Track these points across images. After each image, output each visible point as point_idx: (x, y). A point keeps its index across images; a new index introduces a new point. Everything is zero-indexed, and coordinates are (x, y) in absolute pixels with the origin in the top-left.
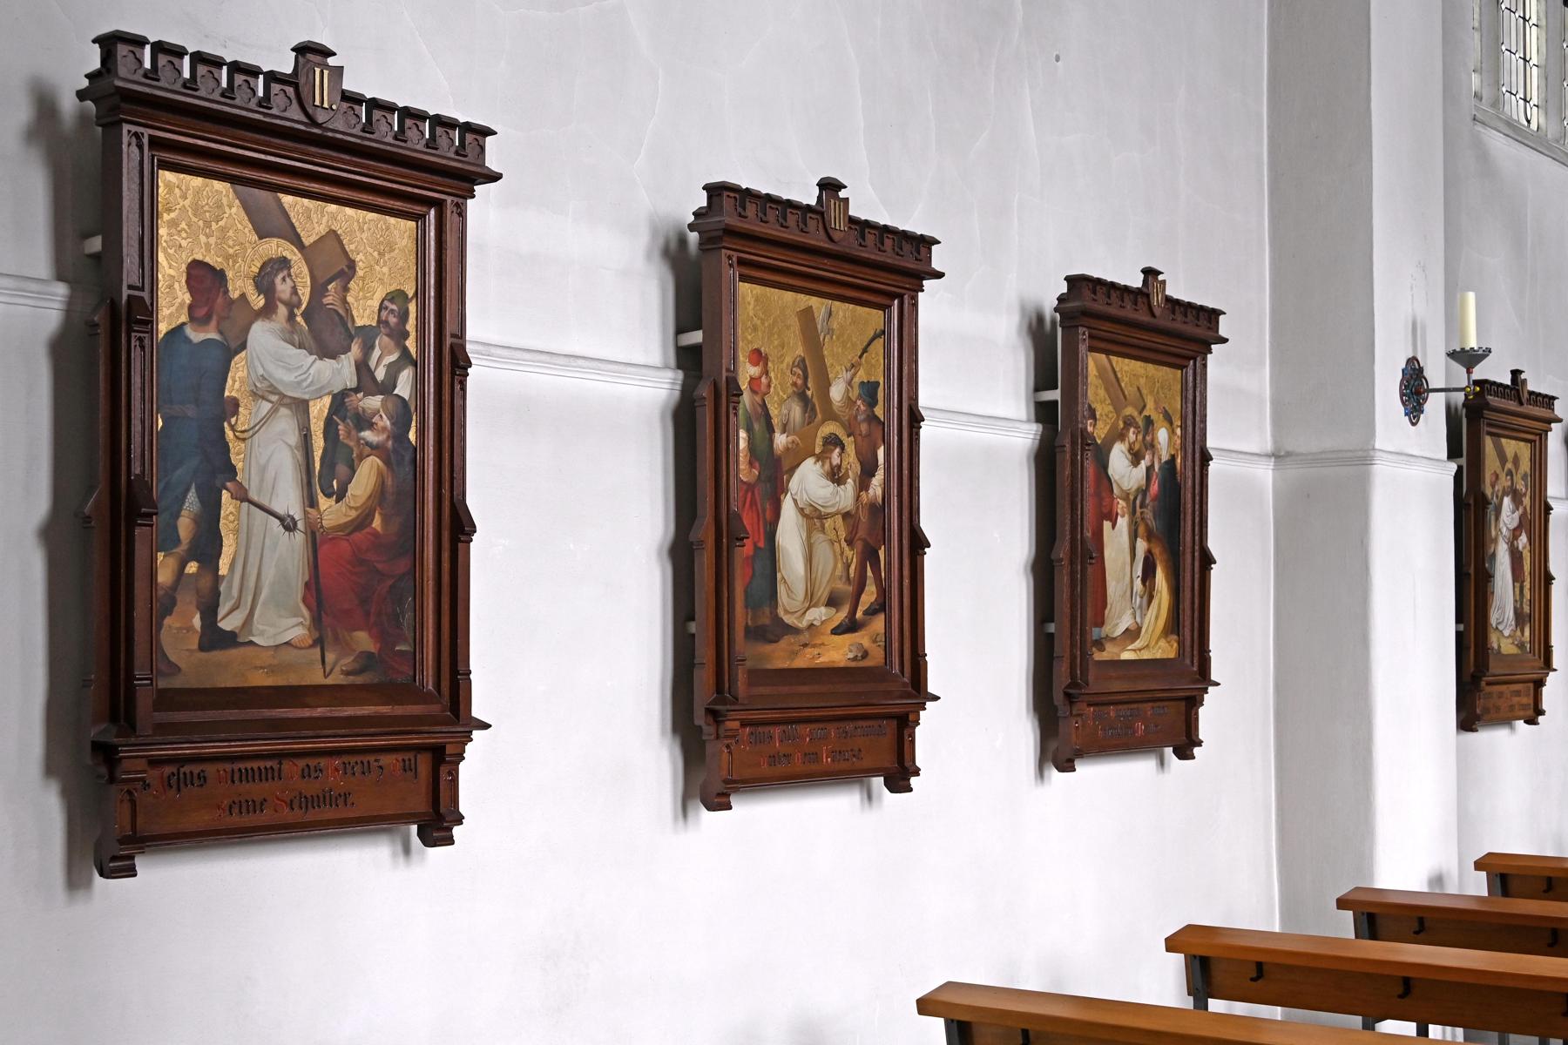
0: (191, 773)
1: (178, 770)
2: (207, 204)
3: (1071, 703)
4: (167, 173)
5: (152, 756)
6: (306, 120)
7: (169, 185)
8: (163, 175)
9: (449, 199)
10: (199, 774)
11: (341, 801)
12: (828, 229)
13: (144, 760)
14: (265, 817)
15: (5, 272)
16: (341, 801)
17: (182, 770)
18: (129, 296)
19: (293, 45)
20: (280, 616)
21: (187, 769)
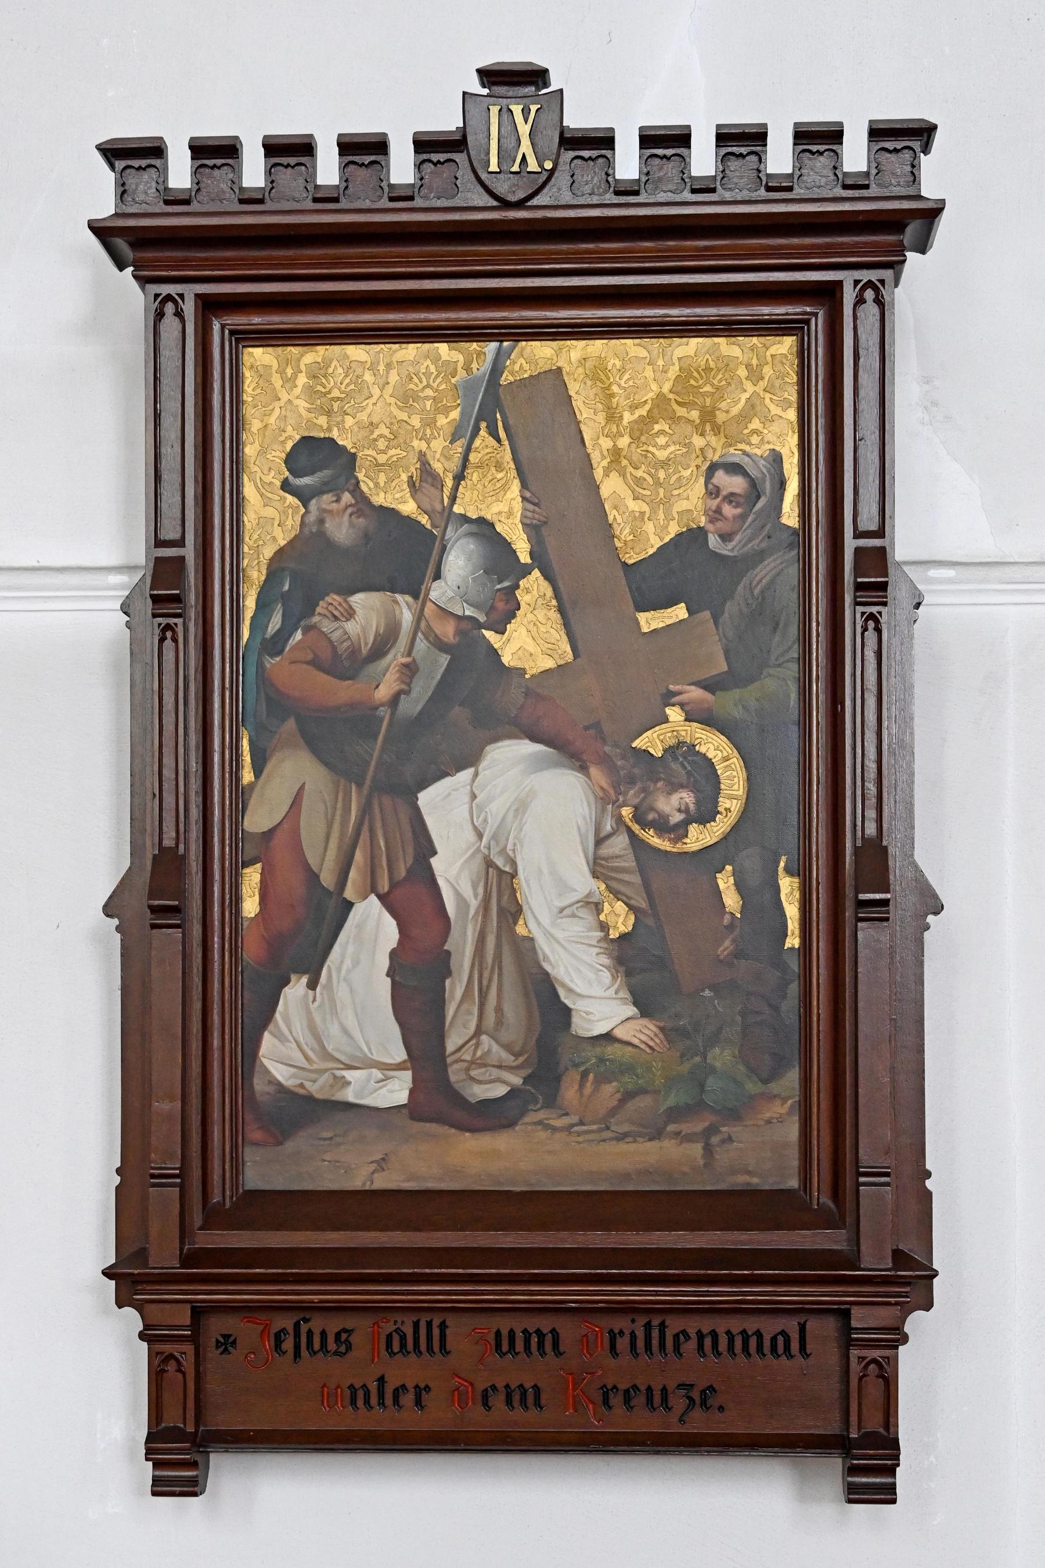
0: (759, 1334)
1: (297, 1326)
2: (428, 386)
3: (859, 1358)
4: (258, 352)
5: (197, 1301)
6: (495, 203)
7: (264, 374)
8: (251, 354)
9: (847, 277)
10: (338, 1335)
11: (408, 1399)
12: (484, 176)
13: (188, 1306)
14: (409, 1418)
15: (7, 564)
16: (408, 1399)
17: (304, 1328)
18: (858, 551)
19: (478, 67)
20: (302, 1085)
21: (317, 1324)
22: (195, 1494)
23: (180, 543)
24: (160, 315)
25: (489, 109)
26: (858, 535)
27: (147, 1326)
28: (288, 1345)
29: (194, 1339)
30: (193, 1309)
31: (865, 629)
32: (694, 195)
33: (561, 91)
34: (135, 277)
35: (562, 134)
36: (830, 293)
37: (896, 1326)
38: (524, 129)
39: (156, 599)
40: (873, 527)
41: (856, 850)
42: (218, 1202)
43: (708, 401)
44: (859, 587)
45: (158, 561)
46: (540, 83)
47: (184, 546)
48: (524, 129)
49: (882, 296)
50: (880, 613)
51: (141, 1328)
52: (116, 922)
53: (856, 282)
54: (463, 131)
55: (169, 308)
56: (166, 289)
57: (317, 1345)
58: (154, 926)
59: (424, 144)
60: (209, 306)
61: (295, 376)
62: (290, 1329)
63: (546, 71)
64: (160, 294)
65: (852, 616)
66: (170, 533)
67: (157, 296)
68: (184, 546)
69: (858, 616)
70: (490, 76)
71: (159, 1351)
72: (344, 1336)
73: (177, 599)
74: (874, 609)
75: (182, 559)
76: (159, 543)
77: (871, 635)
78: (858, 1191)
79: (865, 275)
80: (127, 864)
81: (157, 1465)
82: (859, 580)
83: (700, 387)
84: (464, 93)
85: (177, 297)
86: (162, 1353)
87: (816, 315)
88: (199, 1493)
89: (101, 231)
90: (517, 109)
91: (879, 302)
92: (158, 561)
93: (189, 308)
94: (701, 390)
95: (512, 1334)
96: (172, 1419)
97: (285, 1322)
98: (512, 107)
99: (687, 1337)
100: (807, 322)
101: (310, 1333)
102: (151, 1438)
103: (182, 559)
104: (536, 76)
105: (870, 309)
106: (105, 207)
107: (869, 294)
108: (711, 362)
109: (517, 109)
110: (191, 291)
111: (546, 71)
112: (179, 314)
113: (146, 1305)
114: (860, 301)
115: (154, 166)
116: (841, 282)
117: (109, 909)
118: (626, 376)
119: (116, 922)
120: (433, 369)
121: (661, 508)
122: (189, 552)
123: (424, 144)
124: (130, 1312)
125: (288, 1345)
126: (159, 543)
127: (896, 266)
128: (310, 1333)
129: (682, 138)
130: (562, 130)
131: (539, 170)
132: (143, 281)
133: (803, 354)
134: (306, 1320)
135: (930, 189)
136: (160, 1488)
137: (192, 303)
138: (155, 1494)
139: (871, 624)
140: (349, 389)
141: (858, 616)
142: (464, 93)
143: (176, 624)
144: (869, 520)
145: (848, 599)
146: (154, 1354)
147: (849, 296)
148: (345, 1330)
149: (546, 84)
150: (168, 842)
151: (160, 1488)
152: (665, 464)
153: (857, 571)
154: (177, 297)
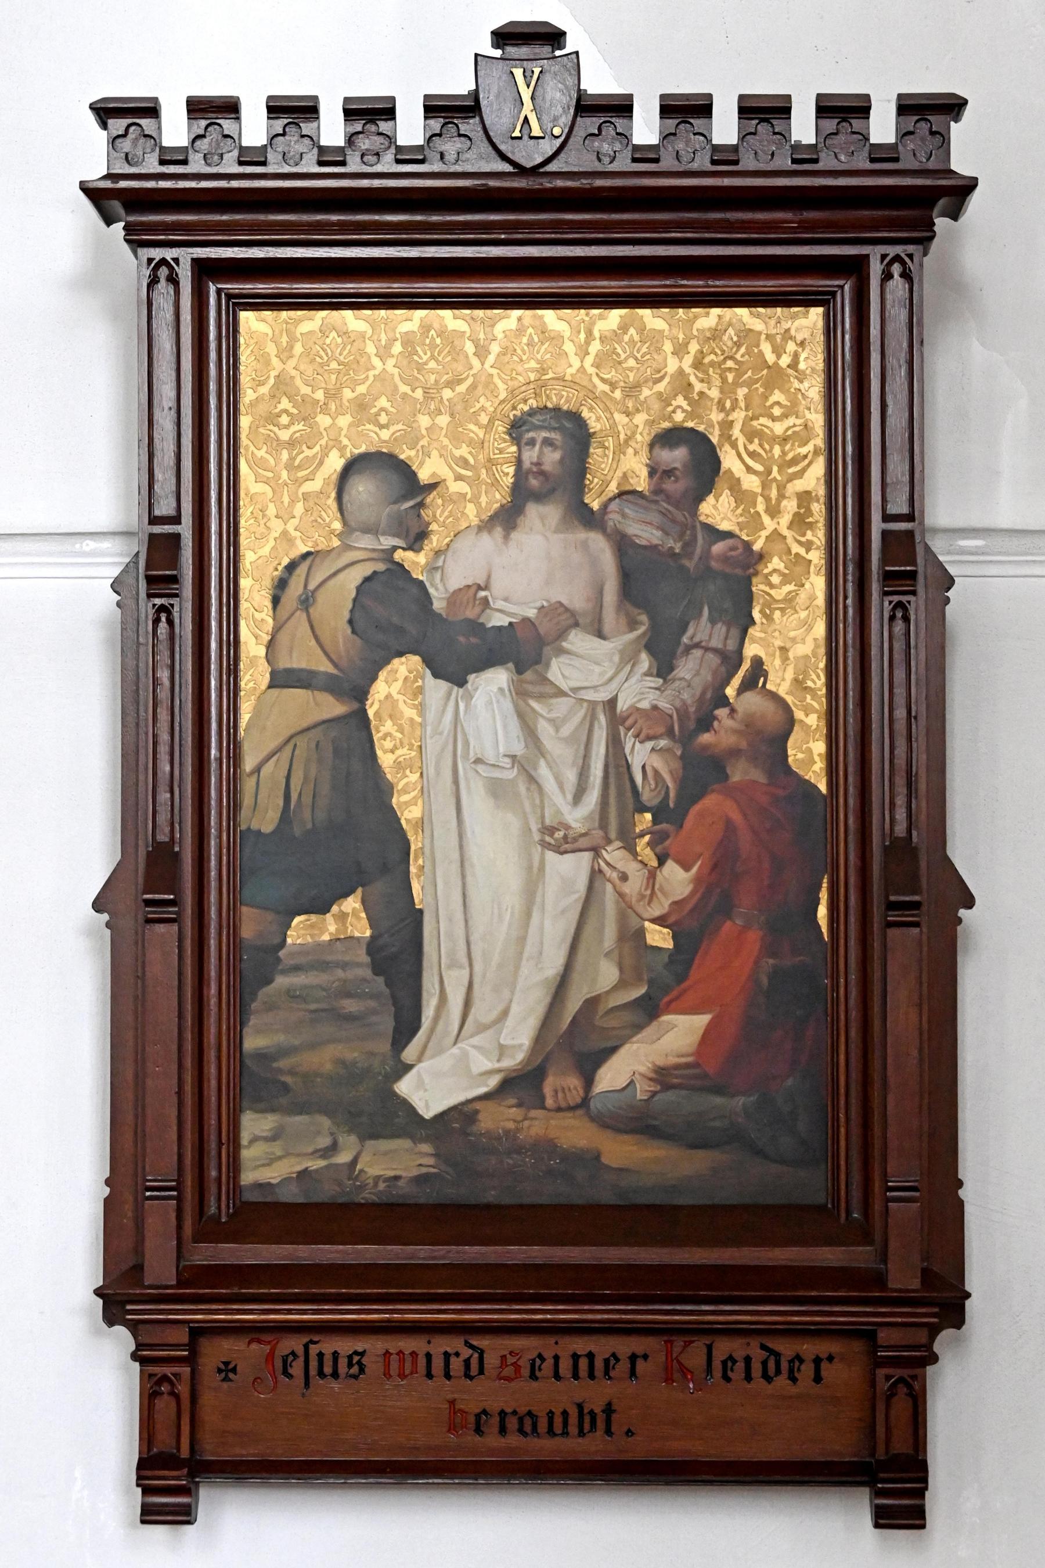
1: (306, 1347)
9: (874, 253)
17: (314, 1350)
21: (329, 1345)
22: (189, 1523)
23: (176, 520)
24: (153, 281)
25: (512, 73)
26: (887, 518)
27: (139, 1346)
28: (297, 1369)
29: (191, 1360)
30: (190, 1328)
31: (892, 618)
32: (635, 165)
33: (577, 53)
34: (126, 240)
35: (579, 100)
36: (857, 268)
37: (705, 1350)
38: (526, 94)
39: (150, 580)
40: (905, 510)
41: (886, 850)
42: (214, 1214)
43: (631, 375)
44: (888, 577)
45: (152, 536)
46: (556, 45)
47: (180, 523)
48: (526, 94)
49: (177, 275)
50: (909, 602)
51: (133, 1348)
52: (105, 917)
53: (883, 257)
54: (475, 95)
55: (164, 272)
56: (157, 253)
57: (328, 1369)
58: (148, 921)
59: (433, 108)
60: (204, 270)
61: (588, 343)
62: (300, 1350)
63: (563, 34)
64: (154, 259)
65: (879, 605)
66: (165, 507)
67: (150, 261)
68: (180, 523)
69: (886, 603)
70: (503, 37)
71: (154, 1372)
72: (356, 1359)
73: (175, 579)
74: (904, 598)
75: (177, 536)
76: (154, 520)
77: (899, 627)
78: (887, 1207)
79: (892, 250)
80: (119, 857)
81: (147, 1491)
82: (887, 568)
83: (426, 364)
84: (476, 55)
85: (172, 262)
86: (155, 1375)
87: (842, 287)
88: (192, 1520)
89: (93, 193)
90: (518, 73)
91: (906, 275)
92: (152, 536)
93: (185, 273)
94: (426, 367)
95: (335, 1355)
96: (164, 1442)
97: (294, 1343)
98: (514, 70)
99: (734, 1362)
100: (833, 294)
101: (321, 1355)
102: (143, 1465)
103: (177, 536)
104: (554, 37)
105: (897, 283)
106: (95, 170)
107: (896, 269)
108: (534, 336)
109: (518, 73)
110: (186, 256)
111: (563, 34)
112: (173, 280)
113: (140, 1327)
114: (887, 276)
115: (138, 125)
116: (867, 256)
117: (98, 905)
118: (743, 350)
119: (105, 917)
120: (636, 338)
121: (286, 492)
122: (186, 529)
123: (433, 108)
124: (121, 1330)
125: (297, 1369)
126: (154, 520)
127: (926, 240)
128: (321, 1355)
129: (230, 107)
130: (581, 94)
131: (542, 135)
132: (135, 244)
133: (829, 331)
134: (312, 1342)
135: (961, 163)
136: (149, 1515)
137: (189, 267)
138: (143, 1522)
139: (163, 617)
140: (645, 359)
141: (886, 603)
142: (476, 55)
143: (909, 602)
144: (899, 505)
145: (875, 587)
146: (146, 1376)
147: (876, 269)
148: (356, 1353)
149: (561, 47)
150: (900, 830)
151: (149, 1515)
152: (291, 444)
153: (884, 560)
154: (172, 262)
